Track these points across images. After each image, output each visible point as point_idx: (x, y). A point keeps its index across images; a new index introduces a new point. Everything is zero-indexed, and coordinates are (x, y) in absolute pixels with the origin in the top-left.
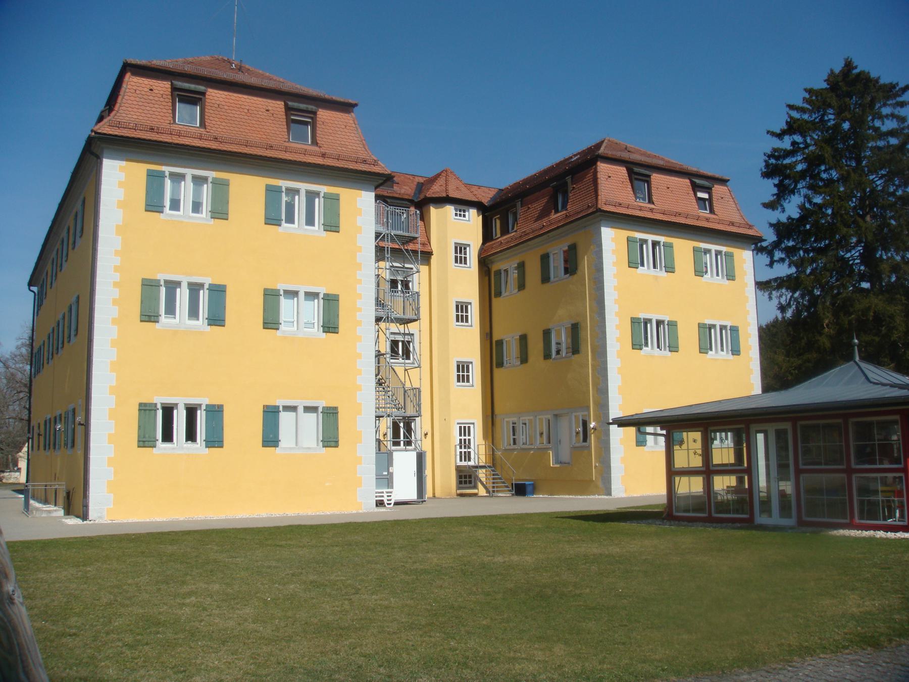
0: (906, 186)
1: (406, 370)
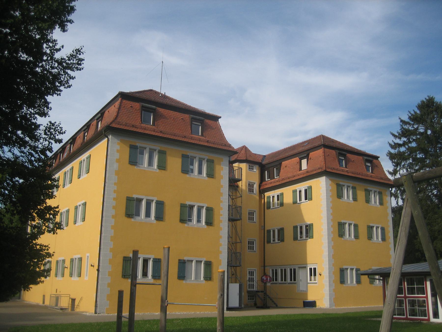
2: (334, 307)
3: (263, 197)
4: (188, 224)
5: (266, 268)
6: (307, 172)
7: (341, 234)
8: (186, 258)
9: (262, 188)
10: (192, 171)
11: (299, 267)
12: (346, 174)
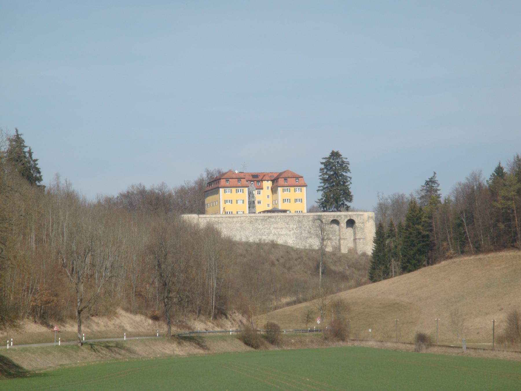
0: (2, 339)
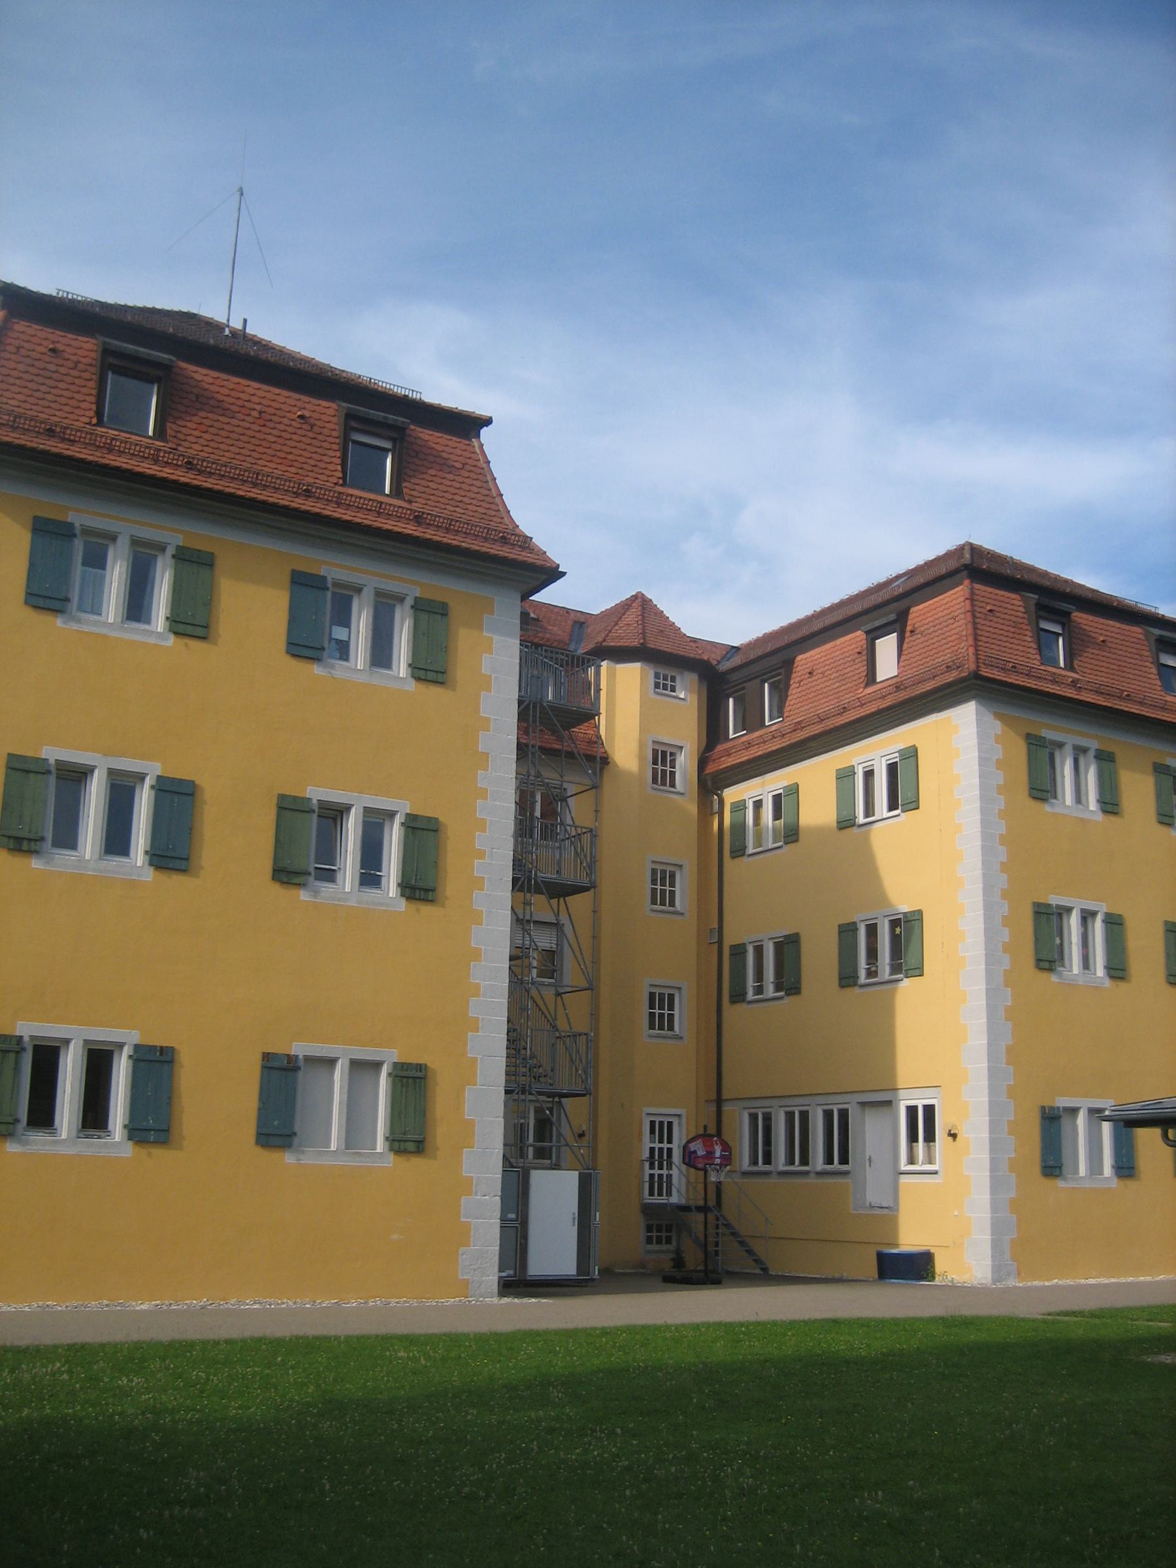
1: (559, 994)
2: (1012, 1282)
3: (716, 807)
4: (316, 893)
5: (727, 1108)
6: (898, 687)
7: (1048, 958)
8: (300, 1049)
9: (711, 769)
10: (343, 650)
11: (863, 1104)
12: (1070, 693)
